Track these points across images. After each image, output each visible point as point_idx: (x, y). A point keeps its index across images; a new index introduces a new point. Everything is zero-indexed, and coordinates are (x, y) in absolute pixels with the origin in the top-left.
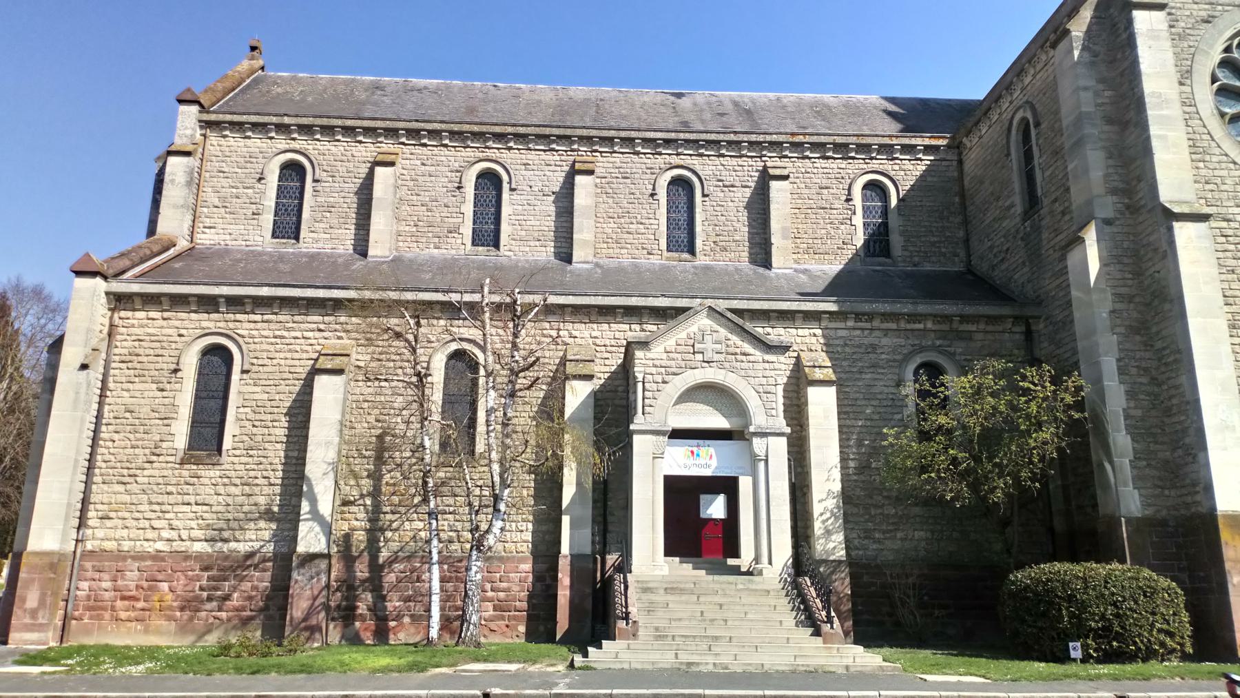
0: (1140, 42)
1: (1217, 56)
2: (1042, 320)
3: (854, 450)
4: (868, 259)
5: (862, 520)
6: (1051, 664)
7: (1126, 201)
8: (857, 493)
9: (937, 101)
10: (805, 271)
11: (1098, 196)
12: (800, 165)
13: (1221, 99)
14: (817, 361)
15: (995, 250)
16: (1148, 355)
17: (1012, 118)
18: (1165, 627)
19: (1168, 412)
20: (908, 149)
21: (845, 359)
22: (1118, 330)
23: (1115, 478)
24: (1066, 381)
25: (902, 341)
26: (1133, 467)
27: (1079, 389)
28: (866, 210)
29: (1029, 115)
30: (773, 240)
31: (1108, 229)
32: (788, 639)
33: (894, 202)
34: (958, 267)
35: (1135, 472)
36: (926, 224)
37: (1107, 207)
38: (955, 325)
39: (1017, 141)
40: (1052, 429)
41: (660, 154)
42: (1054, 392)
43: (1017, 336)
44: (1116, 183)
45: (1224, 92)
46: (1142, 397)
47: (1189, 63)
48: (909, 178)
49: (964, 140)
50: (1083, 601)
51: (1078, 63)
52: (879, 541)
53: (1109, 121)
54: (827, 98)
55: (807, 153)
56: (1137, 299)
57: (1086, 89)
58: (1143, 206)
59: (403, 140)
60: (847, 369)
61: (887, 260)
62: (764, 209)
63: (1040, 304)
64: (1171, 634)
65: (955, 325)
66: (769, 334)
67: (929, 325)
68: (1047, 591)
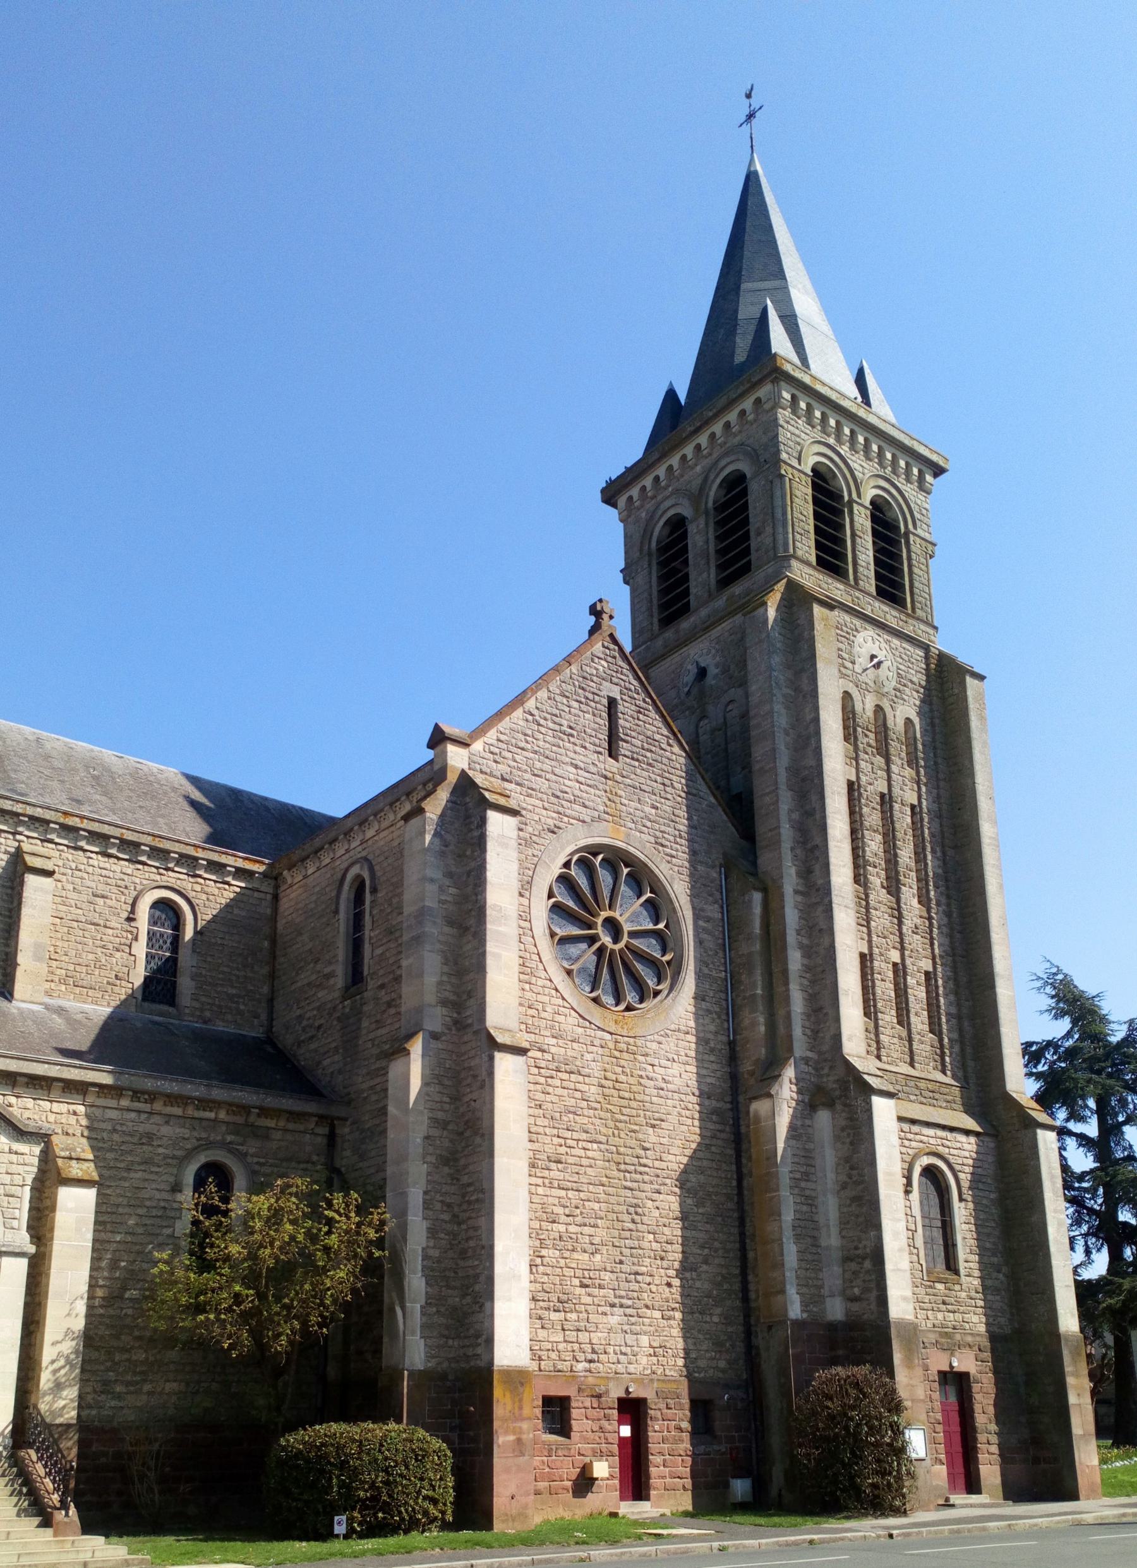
0: (491, 846)
1: (557, 870)
2: (348, 1123)
3: (106, 1274)
4: (146, 1004)
5: (102, 1368)
6: (312, 1543)
7: (455, 1015)
8: (100, 1333)
9: (251, 797)
10: (60, 1011)
11: (430, 1005)
12: (70, 857)
13: (555, 916)
14: (75, 1151)
15: (305, 1023)
16: (453, 1189)
17: (347, 870)
18: (430, 1493)
19: (463, 1254)
20: (216, 867)
21: (111, 1150)
22: (429, 1159)
23: (404, 1323)
24: (372, 1213)
25: (186, 1133)
26: (423, 1314)
27: (383, 1223)
28: (151, 936)
29: (366, 875)
30: (20, 959)
31: (434, 1044)
32: (9, 1533)
33: (189, 933)
34: (257, 1032)
35: (424, 1319)
36: (225, 969)
37: (435, 1020)
38: (252, 1119)
39: (348, 899)
40: (349, 1266)
42: (359, 1225)
43: (319, 1140)
44: (447, 993)
45: (557, 909)
46: (442, 1235)
47: (531, 873)
48: (212, 905)
49: (285, 873)
50: (356, 1468)
51: (428, 849)
52: (119, 1397)
53: (450, 923)
54: (108, 755)
55: (82, 844)
56: (450, 1127)
57: (432, 880)
58: (470, 1025)
60: (112, 1164)
61: (171, 1009)
62: (10, 910)
63: (349, 1103)
64: (434, 1501)
65: (252, 1119)
66: (10, 1105)
67: (222, 1115)
68: (320, 1457)
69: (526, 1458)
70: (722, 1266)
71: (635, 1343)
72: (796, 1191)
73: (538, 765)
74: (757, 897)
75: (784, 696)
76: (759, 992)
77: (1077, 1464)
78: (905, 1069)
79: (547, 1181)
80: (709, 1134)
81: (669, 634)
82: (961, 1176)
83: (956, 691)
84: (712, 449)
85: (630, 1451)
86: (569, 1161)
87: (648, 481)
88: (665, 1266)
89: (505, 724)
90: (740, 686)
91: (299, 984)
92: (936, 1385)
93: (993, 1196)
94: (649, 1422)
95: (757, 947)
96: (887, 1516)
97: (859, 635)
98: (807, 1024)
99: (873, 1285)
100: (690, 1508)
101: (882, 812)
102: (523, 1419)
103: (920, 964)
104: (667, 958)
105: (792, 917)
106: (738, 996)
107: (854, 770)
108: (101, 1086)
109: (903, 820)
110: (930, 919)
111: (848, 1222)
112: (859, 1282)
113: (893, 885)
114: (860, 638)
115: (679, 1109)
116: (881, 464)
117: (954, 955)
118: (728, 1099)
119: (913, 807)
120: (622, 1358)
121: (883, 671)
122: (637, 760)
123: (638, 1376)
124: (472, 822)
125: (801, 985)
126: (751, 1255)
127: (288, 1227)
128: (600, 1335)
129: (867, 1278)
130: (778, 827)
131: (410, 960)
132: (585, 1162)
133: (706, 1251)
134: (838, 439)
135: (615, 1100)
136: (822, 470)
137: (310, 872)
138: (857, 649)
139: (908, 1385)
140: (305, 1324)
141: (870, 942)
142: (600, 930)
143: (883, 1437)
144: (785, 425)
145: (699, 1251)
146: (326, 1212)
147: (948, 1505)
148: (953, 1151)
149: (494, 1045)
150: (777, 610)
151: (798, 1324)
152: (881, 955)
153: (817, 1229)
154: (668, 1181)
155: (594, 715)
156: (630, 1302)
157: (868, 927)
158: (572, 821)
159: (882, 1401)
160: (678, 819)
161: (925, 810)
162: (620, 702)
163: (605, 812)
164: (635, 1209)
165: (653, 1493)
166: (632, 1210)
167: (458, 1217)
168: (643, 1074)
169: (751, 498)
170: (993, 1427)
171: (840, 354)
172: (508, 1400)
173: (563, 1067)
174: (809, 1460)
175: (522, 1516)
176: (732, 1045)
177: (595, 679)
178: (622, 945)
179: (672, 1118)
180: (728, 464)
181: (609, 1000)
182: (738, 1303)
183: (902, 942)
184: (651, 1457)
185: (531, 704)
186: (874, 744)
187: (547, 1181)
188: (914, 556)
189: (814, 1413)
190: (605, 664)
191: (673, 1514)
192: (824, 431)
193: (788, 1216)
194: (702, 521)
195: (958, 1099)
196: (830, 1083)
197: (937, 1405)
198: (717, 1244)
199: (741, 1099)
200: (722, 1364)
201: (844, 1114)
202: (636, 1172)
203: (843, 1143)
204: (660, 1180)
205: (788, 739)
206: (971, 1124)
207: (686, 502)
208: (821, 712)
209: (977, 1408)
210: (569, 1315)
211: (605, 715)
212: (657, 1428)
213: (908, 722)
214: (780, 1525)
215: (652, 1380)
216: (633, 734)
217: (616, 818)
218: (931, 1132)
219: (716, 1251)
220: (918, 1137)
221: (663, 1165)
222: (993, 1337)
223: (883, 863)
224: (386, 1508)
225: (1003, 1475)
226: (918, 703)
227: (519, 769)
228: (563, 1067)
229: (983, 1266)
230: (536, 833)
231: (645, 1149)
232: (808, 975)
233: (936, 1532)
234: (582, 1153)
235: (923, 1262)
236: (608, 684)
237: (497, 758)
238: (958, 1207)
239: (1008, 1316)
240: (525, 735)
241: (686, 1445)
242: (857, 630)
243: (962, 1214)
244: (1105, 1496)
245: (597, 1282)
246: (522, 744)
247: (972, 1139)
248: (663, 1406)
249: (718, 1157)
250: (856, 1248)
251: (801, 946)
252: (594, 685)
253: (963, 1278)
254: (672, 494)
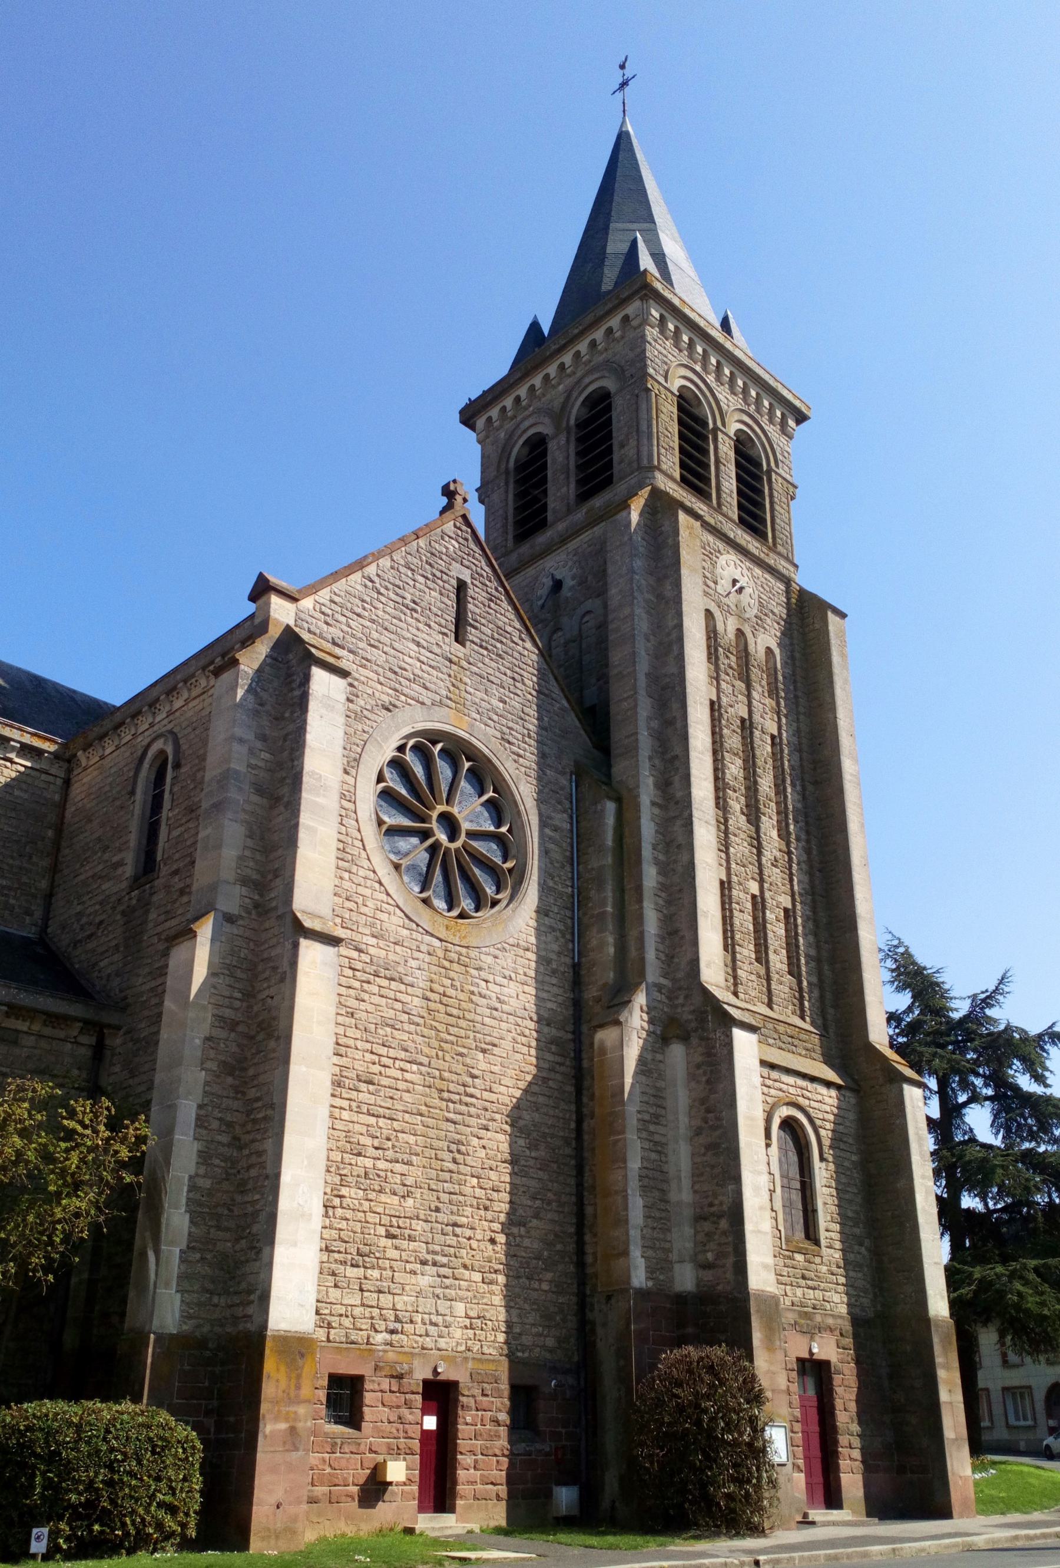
0: (313, 705)
1: (389, 752)
2: (122, 1032)
7: (257, 897)
13: (383, 803)
15: (84, 920)
16: (236, 1105)
18: (168, 1499)
22: (209, 1065)
24: (127, 1127)
26: (182, 1260)
29: (169, 750)
31: (227, 928)
34: (29, 932)
37: (232, 899)
43: (83, 1051)
45: (387, 795)
46: (217, 1162)
47: (359, 750)
49: (80, 753)
50: (69, 1462)
51: (240, 705)
53: (260, 790)
56: (241, 1028)
57: (241, 741)
58: (276, 908)
63: (123, 1010)
64: (172, 1510)
69: (301, 1453)
70: (556, 1222)
71: (448, 1312)
72: (644, 1135)
73: (375, 635)
74: (610, 807)
75: (647, 601)
76: (609, 909)
77: (950, 1474)
78: (764, 1010)
79: (354, 1104)
80: (546, 1066)
81: (525, 549)
82: (823, 1132)
83: (817, 626)
84: (576, 368)
85: (434, 1448)
86: (383, 1083)
87: (508, 402)
88: (489, 1218)
89: (341, 585)
90: (599, 596)
91: (82, 877)
92: (794, 1374)
93: (854, 1158)
94: (460, 1412)
95: (609, 860)
96: (744, 1536)
97: (721, 557)
98: (661, 947)
99: (730, 1249)
100: (503, 1523)
101: (743, 738)
102: (298, 1401)
103: (779, 899)
104: (509, 865)
105: (648, 830)
106: (585, 914)
107: (714, 690)
109: (764, 749)
110: (789, 853)
111: (702, 1174)
112: (712, 1245)
113: (753, 814)
114: (723, 560)
115: (514, 1034)
116: (745, 400)
117: (813, 894)
118: (570, 1028)
119: (773, 737)
120: (432, 1330)
121: (745, 598)
122: (486, 649)
123: (450, 1353)
124: (294, 681)
125: (656, 904)
126: (589, 1210)
127: (16, 1139)
128: (405, 1298)
129: (723, 1240)
130: (637, 733)
131: (209, 831)
132: (401, 1085)
133: (538, 1203)
134: (705, 367)
135: (441, 1016)
136: (688, 395)
137: (108, 752)
138: (719, 571)
139: (768, 1371)
140: (23, 1263)
141: (728, 869)
142: (434, 825)
143: (741, 1434)
144: (653, 343)
145: (529, 1203)
146: (65, 1122)
147: (807, 1522)
148: (814, 1104)
149: (300, 930)
150: (641, 515)
151: (643, 1294)
152: (740, 884)
153: (666, 1181)
154: (498, 1117)
155: (441, 594)
156: (445, 1260)
157: (727, 853)
158: (410, 701)
159: (740, 1389)
160: (527, 718)
161: (785, 741)
162: (471, 586)
163: (447, 697)
164: (457, 1147)
165: (459, 1503)
166: (454, 1147)
167: (239, 1139)
168: (475, 990)
169: (615, 425)
170: (855, 1428)
171: (706, 298)
172: (282, 1376)
173: (383, 972)
174: (652, 1463)
175: (291, 1531)
176: (576, 968)
177: (444, 557)
178: (458, 844)
179: (507, 1044)
180: (597, 379)
181: (440, 904)
182: (572, 1268)
183: (761, 873)
184: (459, 1457)
185: (371, 570)
186: (735, 667)
187: (354, 1104)
188: (775, 494)
189: (659, 1403)
190: (457, 545)
191: (482, 1531)
192: (690, 356)
193: (634, 1164)
194: (562, 439)
195: (818, 1049)
196: (686, 1014)
197: (795, 1399)
198: (550, 1195)
199: (585, 1028)
200: (550, 1342)
201: (700, 1049)
202: (461, 1102)
203: (698, 1082)
204: (488, 1115)
205: (649, 645)
206: (831, 1075)
207: (547, 420)
208: (685, 618)
209: (839, 1403)
210: (369, 1271)
211: (453, 596)
212: (469, 1419)
213: (769, 650)
214: (617, 1547)
215: (466, 1359)
216: (483, 621)
217: (460, 706)
218: (790, 1080)
219: (549, 1203)
220: (777, 1085)
221: (493, 1097)
222: (856, 1321)
223: (743, 788)
224: (105, 1517)
225: (866, 1486)
226: (778, 634)
227: (353, 636)
228: (383, 972)
229: (846, 1238)
230: (368, 707)
231: (474, 1077)
232: (663, 895)
233: (810, 1558)
234: (398, 1074)
235: (781, 1228)
236: (458, 566)
237: (329, 620)
238: (818, 1166)
239: (871, 1296)
240: (363, 601)
241: (502, 1443)
242: (719, 552)
243: (823, 1174)
244: (978, 1513)
245: (407, 1232)
246: (359, 610)
247: (833, 1093)
248: (477, 1392)
249: (556, 1094)
250: (711, 1205)
251: (657, 862)
252: (443, 564)
253: (824, 1248)
254: (533, 413)
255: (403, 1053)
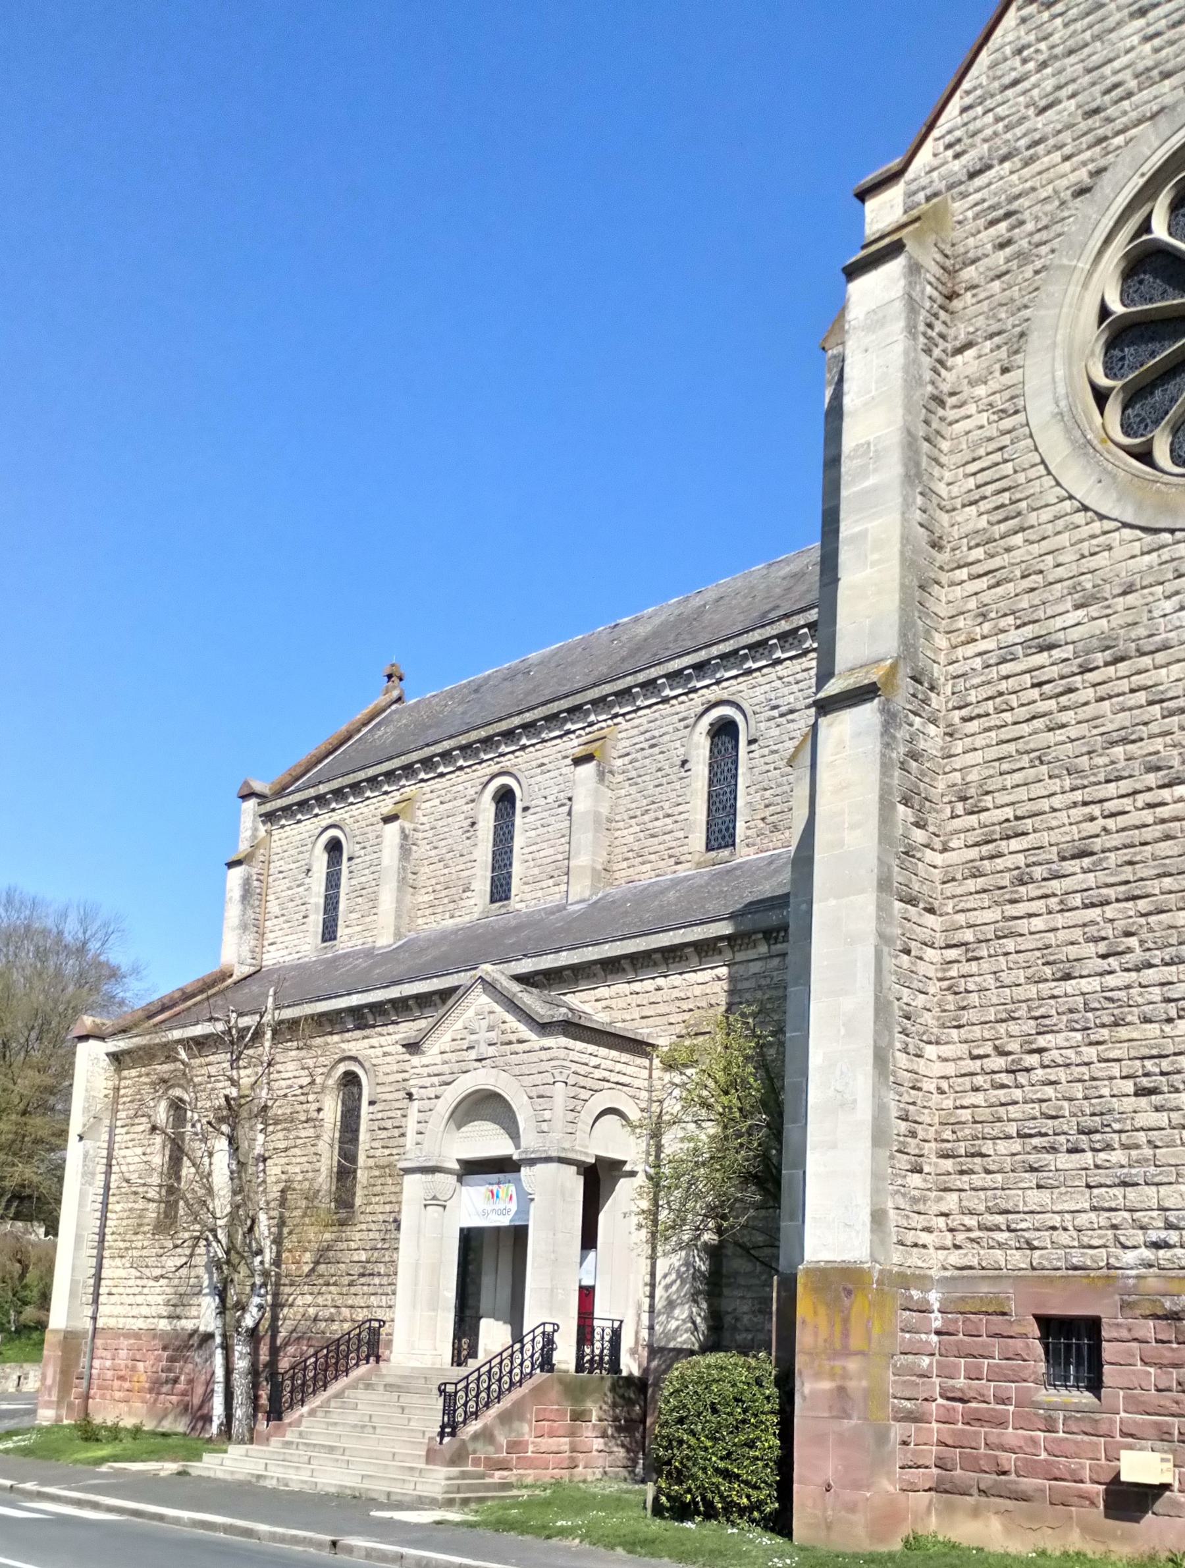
41: (695, 690)
59: (422, 775)
108: (727, 938)
255: (1152, 776)
